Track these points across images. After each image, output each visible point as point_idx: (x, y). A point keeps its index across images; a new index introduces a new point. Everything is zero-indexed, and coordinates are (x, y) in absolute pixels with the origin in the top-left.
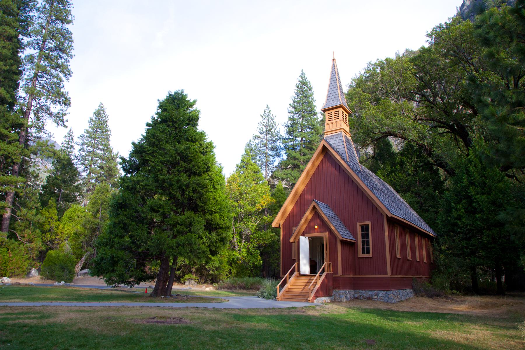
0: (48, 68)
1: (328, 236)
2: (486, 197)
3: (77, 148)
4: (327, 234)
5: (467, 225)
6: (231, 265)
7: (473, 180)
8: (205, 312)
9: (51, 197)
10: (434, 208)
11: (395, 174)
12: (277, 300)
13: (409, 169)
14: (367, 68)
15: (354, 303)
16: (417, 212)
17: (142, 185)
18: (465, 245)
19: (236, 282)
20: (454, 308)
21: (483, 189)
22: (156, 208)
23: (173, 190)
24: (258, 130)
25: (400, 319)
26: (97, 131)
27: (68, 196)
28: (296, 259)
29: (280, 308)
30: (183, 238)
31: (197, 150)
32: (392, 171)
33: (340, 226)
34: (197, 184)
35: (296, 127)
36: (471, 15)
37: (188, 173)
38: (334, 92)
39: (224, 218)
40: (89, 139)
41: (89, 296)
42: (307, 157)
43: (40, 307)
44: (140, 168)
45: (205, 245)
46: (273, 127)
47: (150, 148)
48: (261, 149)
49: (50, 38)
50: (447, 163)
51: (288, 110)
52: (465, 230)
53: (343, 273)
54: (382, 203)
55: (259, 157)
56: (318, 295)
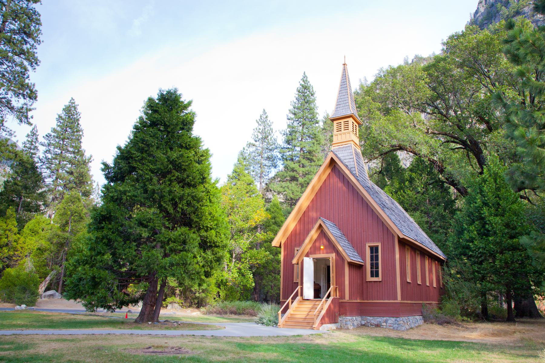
0: (10, 54)
1: (334, 257)
2: (500, 218)
3: (42, 149)
4: (334, 255)
5: (479, 248)
6: (219, 287)
7: (487, 200)
8: (205, 340)
9: (9, 206)
10: (444, 228)
11: (404, 191)
12: (279, 327)
13: (418, 186)
14: (377, 75)
15: (362, 331)
16: (426, 233)
17: (129, 196)
18: (477, 269)
19: (226, 307)
20: (466, 336)
21: (497, 210)
22: (145, 222)
23: (165, 202)
24: (253, 137)
25: (414, 347)
26: (67, 131)
27: (30, 205)
28: (299, 281)
29: (285, 336)
30: (177, 257)
31: (191, 158)
32: (401, 188)
33: (348, 246)
34: (192, 197)
35: (295, 136)
36: (484, 23)
37: (181, 184)
38: (344, 100)
39: (220, 235)
40: (57, 140)
41: (63, 322)
42: (307, 169)
43: (10, 335)
44: (126, 176)
45: (199, 265)
46: (270, 134)
47: (139, 154)
48: (255, 158)
49: (13, 18)
50: (459, 182)
51: (287, 116)
52: (477, 253)
53: (350, 298)
54: (394, 223)
55: (253, 167)
56: (323, 322)
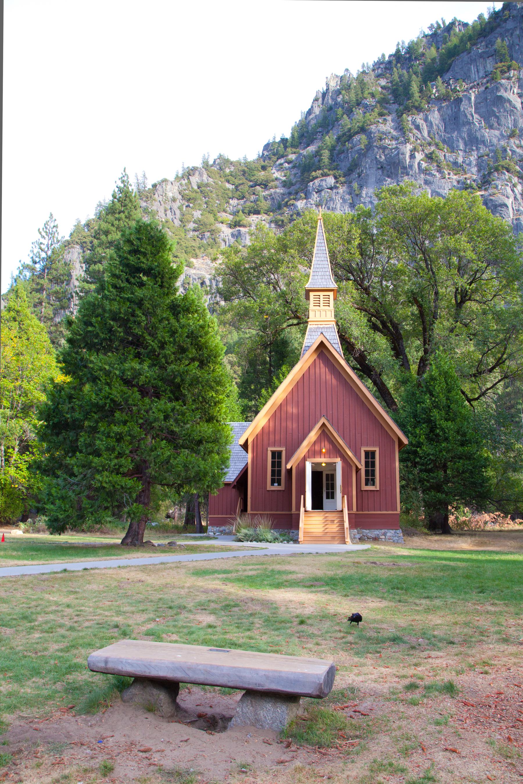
5: (429, 455)
36: (318, 130)
